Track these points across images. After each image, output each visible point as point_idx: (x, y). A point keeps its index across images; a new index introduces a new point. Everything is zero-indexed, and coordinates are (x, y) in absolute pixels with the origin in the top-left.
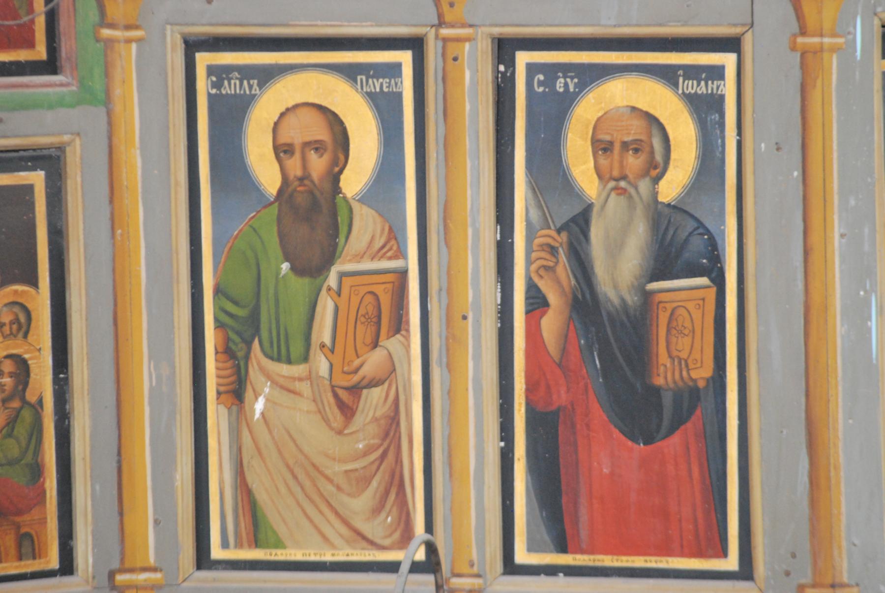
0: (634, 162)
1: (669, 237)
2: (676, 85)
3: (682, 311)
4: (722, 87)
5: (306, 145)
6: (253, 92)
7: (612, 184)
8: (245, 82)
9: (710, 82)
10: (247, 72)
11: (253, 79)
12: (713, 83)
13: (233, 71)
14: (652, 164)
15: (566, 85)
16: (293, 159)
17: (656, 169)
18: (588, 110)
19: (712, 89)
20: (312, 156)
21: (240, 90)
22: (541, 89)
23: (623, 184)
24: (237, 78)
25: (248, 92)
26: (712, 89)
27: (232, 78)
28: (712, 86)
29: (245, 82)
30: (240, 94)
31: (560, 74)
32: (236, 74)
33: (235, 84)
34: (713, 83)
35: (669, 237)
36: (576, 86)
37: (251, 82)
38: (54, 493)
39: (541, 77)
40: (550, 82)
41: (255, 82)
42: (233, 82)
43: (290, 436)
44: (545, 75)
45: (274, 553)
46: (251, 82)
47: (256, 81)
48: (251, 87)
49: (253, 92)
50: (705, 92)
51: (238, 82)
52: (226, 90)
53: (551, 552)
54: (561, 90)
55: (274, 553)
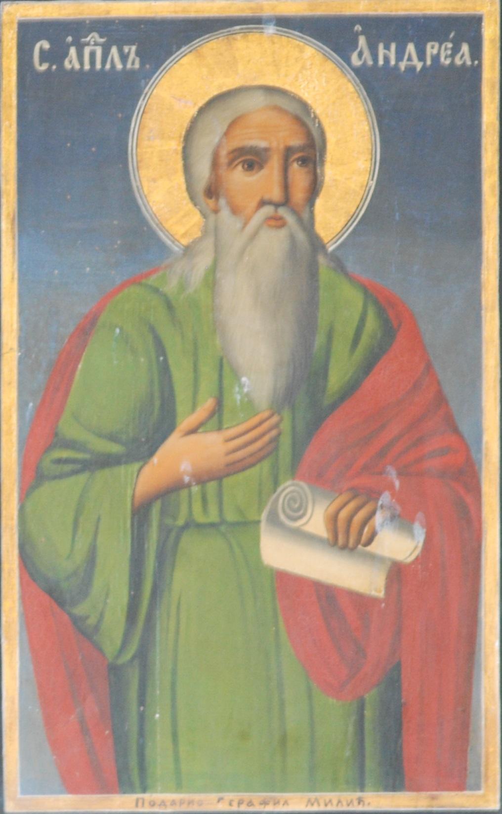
1: (352, 506)
3: (184, 493)
7: (268, 210)
8: (114, 50)
9: (381, 46)
11: (130, 43)
12: (387, 47)
13: (91, 30)
16: (264, 172)
18: (180, 88)
21: (104, 62)
22: (44, 67)
23: (282, 212)
24: (96, 44)
25: (119, 66)
26: (387, 59)
27: (88, 44)
29: (114, 50)
32: (95, 35)
33: (93, 55)
34: (387, 47)
35: (352, 506)
37: (126, 49)
39: (46, 45)
40: (56, 55)
42: (87, 51)
43: (179, 604)
44: (51, 43)
45: (235, 804)
46: (126, 49)
47: (134, 48)
48: (124, 58)
49: (129, 66)
50: (77, 66)
54: (448, 62)
55: (235, 804)
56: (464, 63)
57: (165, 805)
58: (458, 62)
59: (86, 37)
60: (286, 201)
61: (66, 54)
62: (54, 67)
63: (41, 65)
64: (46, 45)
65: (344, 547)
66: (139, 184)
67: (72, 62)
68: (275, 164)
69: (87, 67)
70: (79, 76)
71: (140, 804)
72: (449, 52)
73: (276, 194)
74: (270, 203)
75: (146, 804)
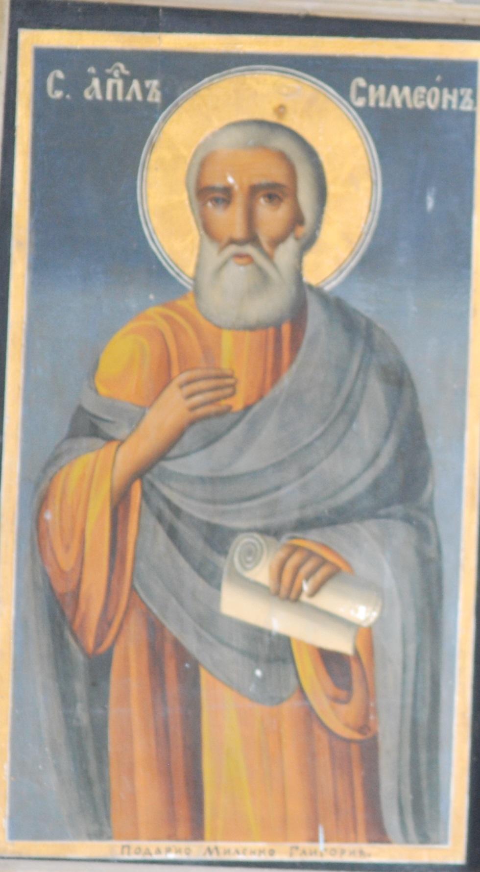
0: (272, 218)
2: (343, 91)
4: (467, 99)
5: (254, 191)
6: (463, 108)
7: (233, 249)
8: (135, 85)
10: (142, 64)
11: (151, 77)
14: (297, 219)
15: (145, 91)
17: (303, 231)
18: (187, 133)
19: (450, 103)
20: (263, 209)
21: (125, 94)
22: (59, 94)
23: (249, 249)
25: (139, 97)
26: (450, 103)
27: (111, 76)
28: (448, 99)
30: (125, 103)
31: (92, 70)
32: (122, 66)
33: (115, 87)
36: (58, 84)
37: (147, 83)
38: (461, 605)
39: (60, 75)
40: (76, 82)
41: (153, 84)
42: (110, 83)
47: (155, 83)
48: (145, 91)
49: (150, 99)
50: (99, 97)
51: (120, 84)
52: (94, 91)
53: (300, 643)
56: (94, 97)
57: (150, 854)
58: (129, 98)
59: (109, 67)
60: (252, 238)
61: (88, 83)
62: (68, 96)
63: (53, 92)
64: (60, 75)
65: (287, 598)
66: (363, 237)
67: (94, 91)
68: (239, 201)
69: (109, 97)
70: (97, 107)
71: (126, 850)
72: (422, 97)
73: (239, 232)
74: (232, 241)
75: (132, 850)
